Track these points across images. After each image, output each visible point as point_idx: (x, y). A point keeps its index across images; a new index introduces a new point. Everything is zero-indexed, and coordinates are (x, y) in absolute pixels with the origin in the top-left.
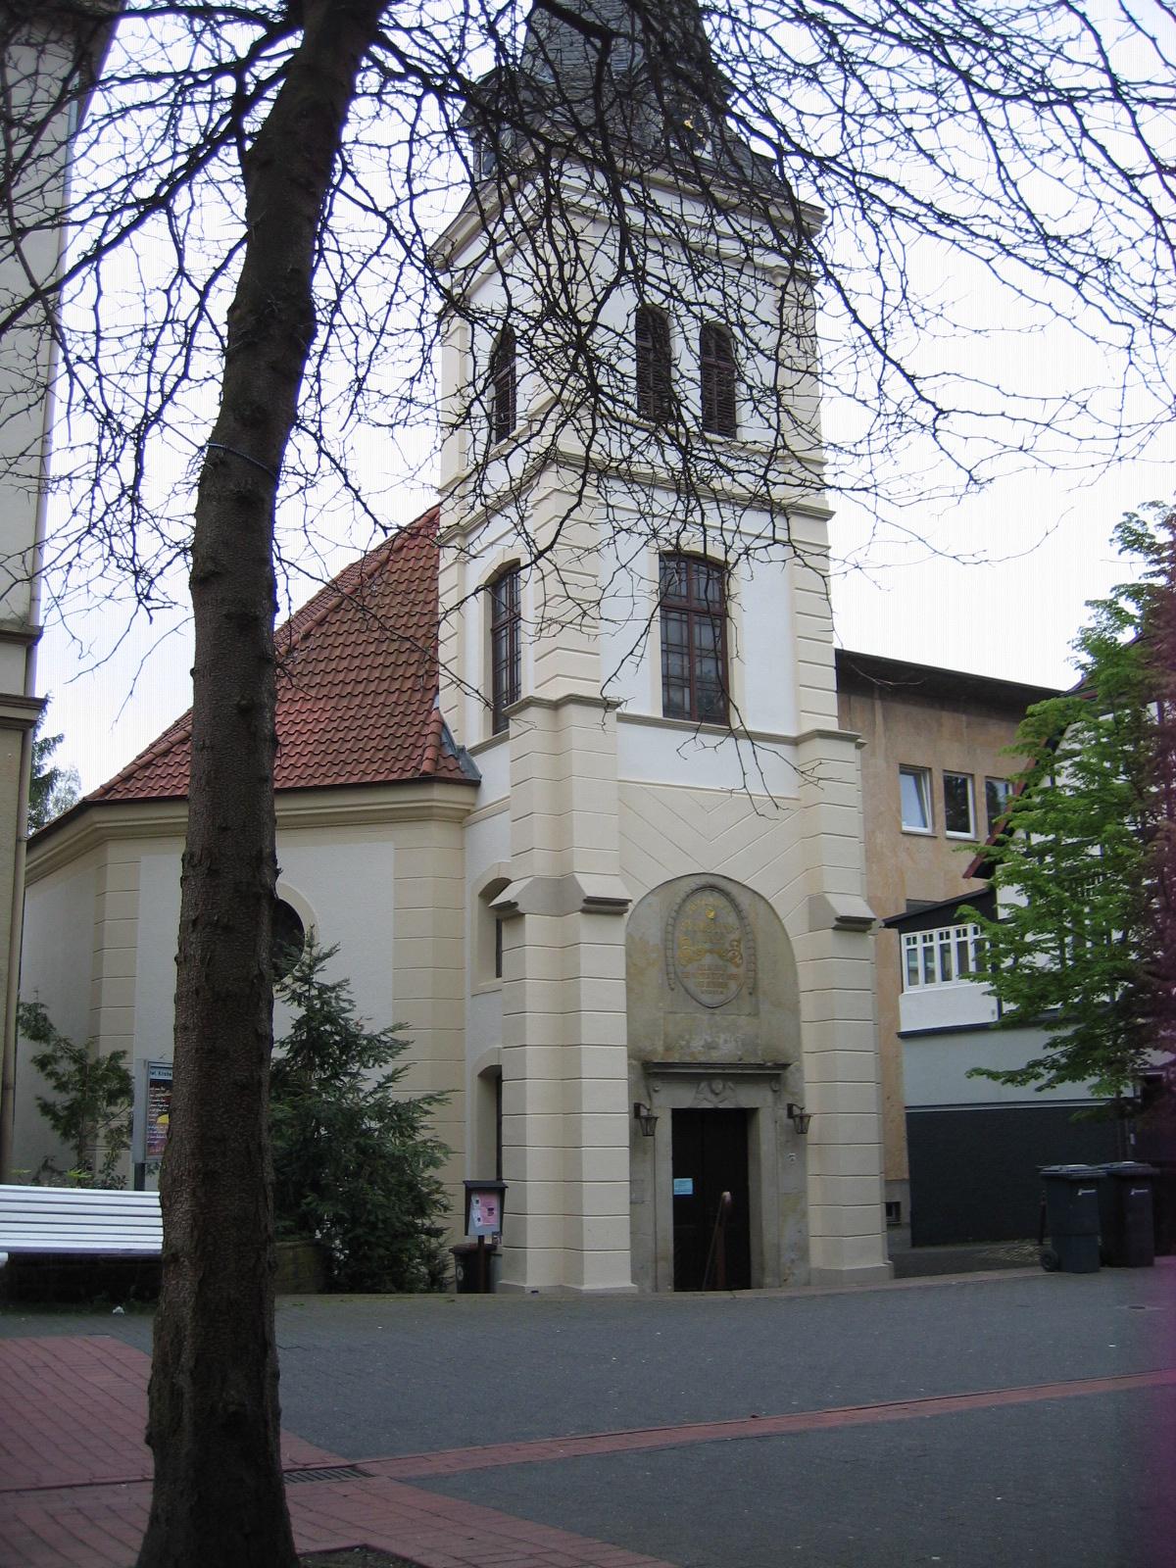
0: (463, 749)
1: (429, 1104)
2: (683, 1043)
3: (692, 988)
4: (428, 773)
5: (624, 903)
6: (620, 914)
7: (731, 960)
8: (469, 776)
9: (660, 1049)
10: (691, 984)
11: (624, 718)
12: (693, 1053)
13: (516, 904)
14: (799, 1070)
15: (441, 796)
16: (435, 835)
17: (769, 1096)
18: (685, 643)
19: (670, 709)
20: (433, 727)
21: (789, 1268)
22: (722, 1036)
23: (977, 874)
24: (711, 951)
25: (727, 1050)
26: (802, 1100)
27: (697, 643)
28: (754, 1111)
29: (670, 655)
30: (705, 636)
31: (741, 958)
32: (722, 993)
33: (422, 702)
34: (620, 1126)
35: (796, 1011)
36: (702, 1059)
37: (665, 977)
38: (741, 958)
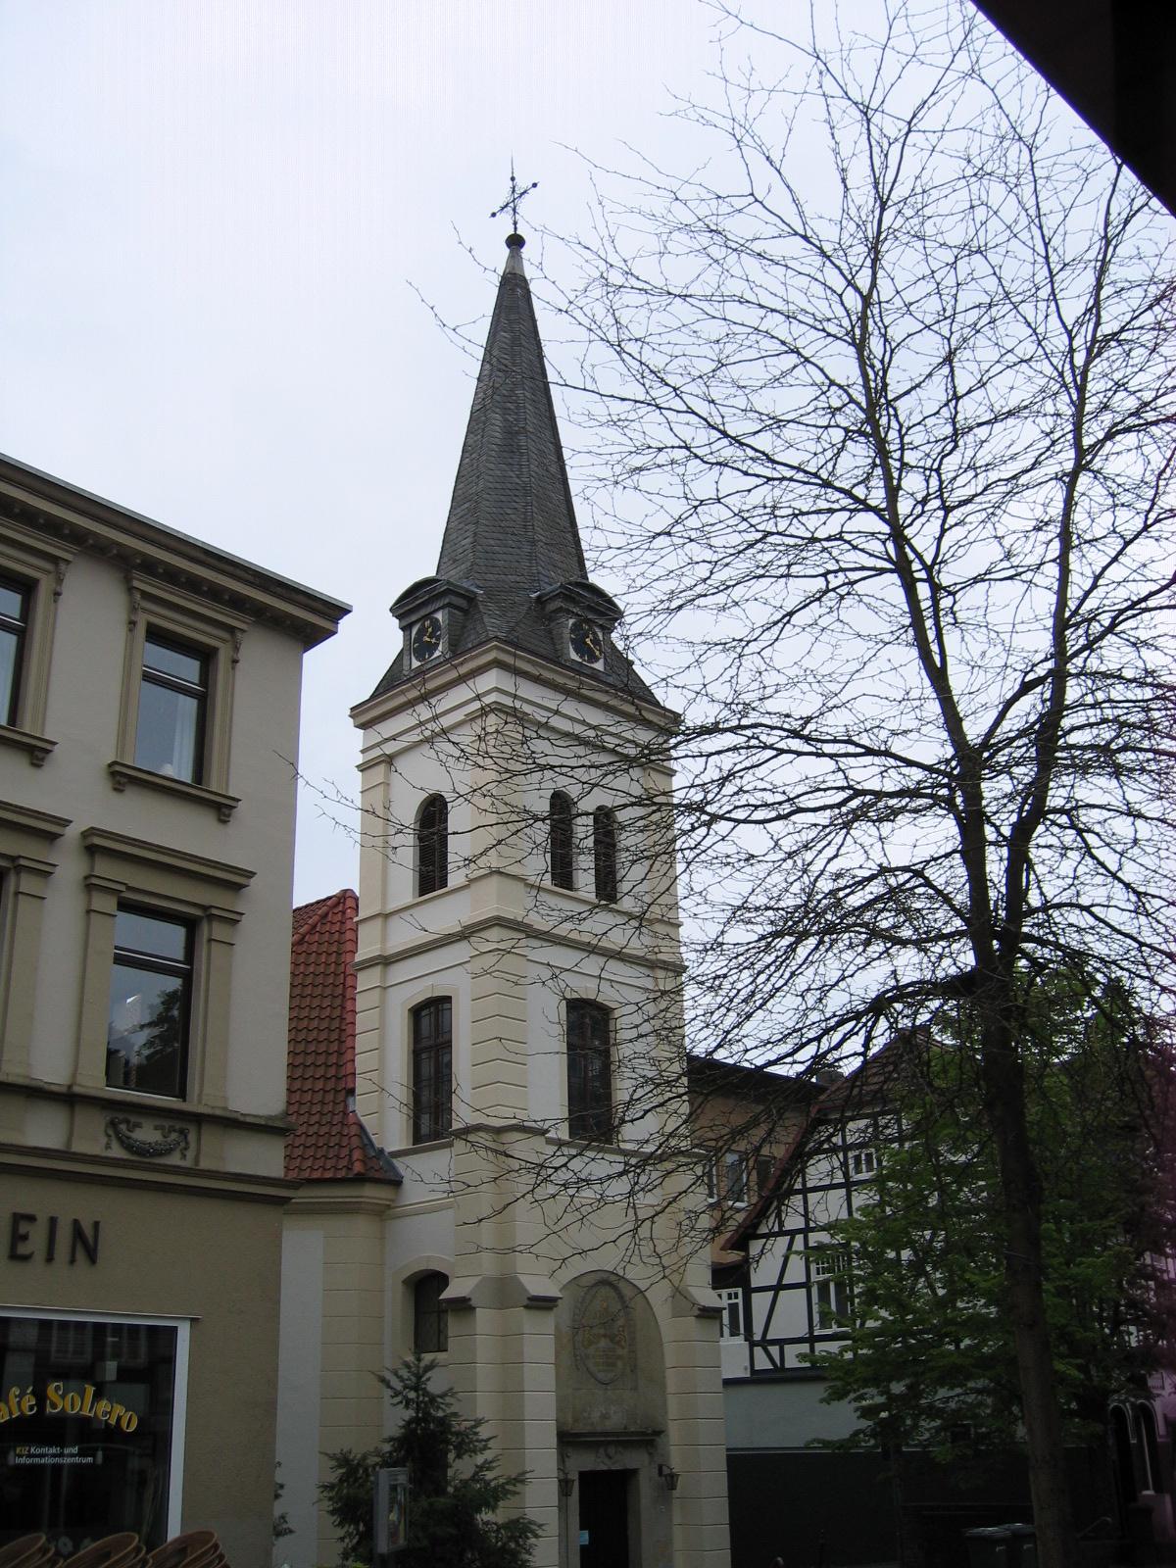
0: (382, 1151)
1: (515, 1485)
2: (585, 1415)
6: (550, 1309)
7: (618, 1343)
8: (391, 1176)
9: (570, 1420)
12: (592, 1424)
15: (371, 1193)
16: (360, 1227)
17: (645, 1457)
20: (354, 1130)
22: (613, 1408)
23: (733, 1248)
24: (605, 1336)
25: (616, 1421)
28: (634, 1472)
34: (553, 1487)
35: (663, 1386)
36: (599, 1429)
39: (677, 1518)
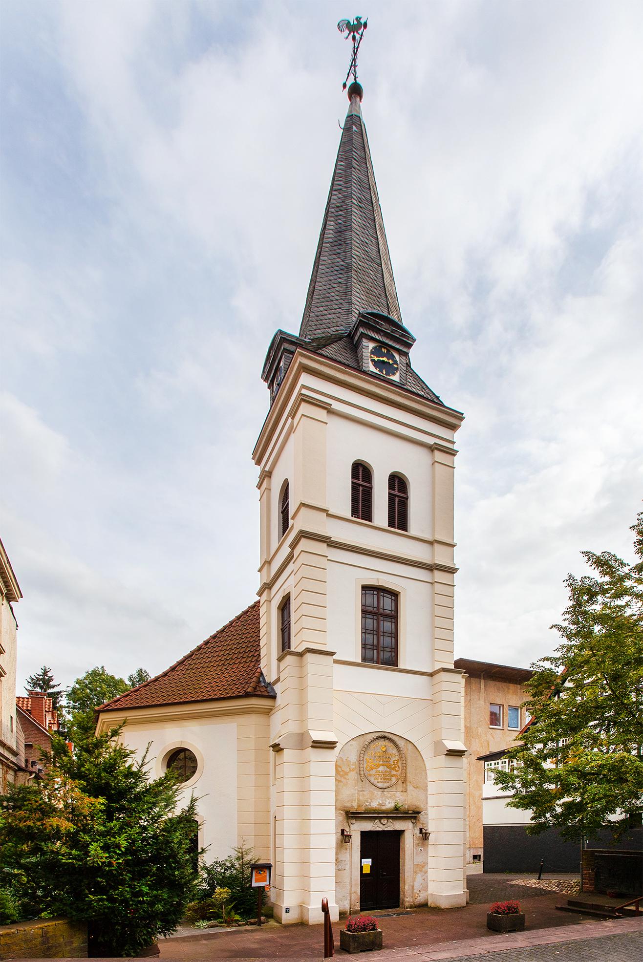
2: (367, 804)
3: (373, 780)
4: (249, 692)
5: (335, 743)
6: (333, 748)
7: (393, 769)
8: (272, 694)
9: (356, 807)
10: (372, 779)
11: (336, 662)
13: (279, 744)
14: (426, 814)
16: (252, 720)
18: (375, 629)
19: (364, 659)
21: (418, 894)
26: (427, 826)
27: (382, 630)
29: (366, 634)
30: (387, 626)
31: (399, 768)
32: (388, 782)
33: (254, 666)
34: (332, 840)
35: (425, 789)
37: (359, 776)
38: (399, 768)
39: (430, 854)
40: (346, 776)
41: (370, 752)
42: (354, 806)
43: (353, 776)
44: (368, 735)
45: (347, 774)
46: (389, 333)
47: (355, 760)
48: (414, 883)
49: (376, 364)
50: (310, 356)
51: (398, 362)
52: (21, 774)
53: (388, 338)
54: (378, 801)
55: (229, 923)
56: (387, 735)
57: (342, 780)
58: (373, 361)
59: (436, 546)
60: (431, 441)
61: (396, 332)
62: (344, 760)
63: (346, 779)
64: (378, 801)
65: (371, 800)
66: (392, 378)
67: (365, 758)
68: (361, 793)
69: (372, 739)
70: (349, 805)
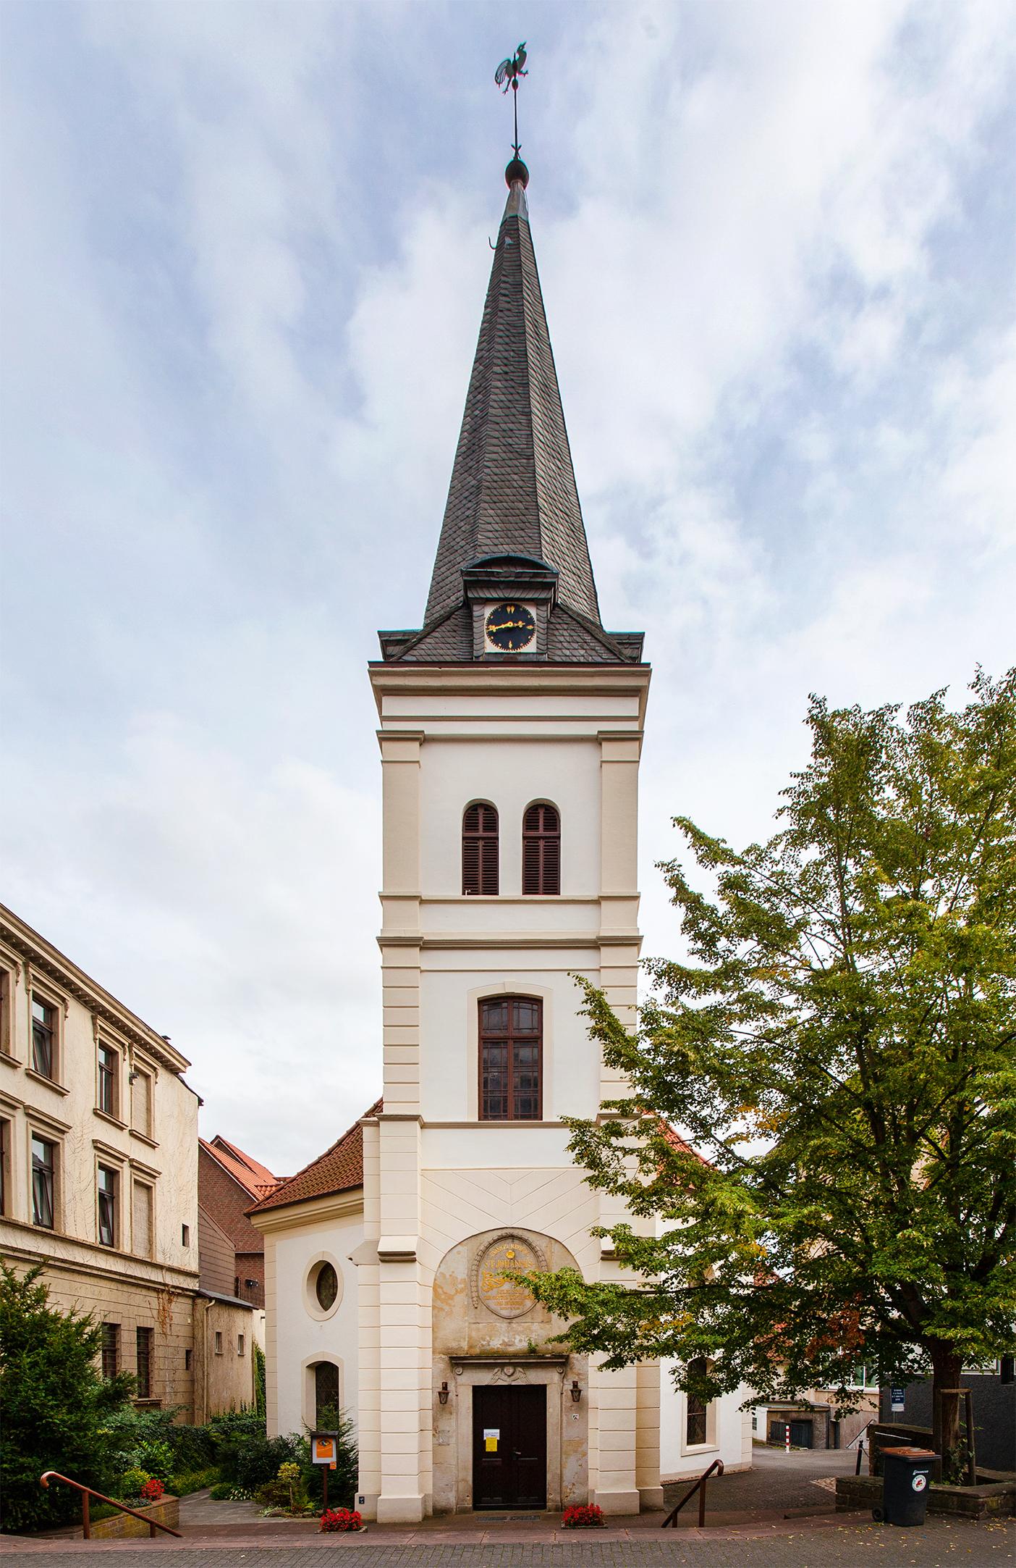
2: (484, 1343)
9: (466, 1348)
10: (492, 1304)
21: (571, 1489)
40: (450, 1302)
41: (489, 1262)
42: (463, 1347)
43: (461, 1300)
44: (486, 1235)
45: (451, 1297)
46: (513, 581)
47: (465, 1276)
48: (564, 1470)
49: (497, 638)
50: (388, 671)
51: (535, 619)
52: (199, 1301)
53: (512, 588)
54: (502, 1337)
55: (298, 1510)
56: (515, 1232)
57: (444, 1307)
58: (490, 634)
59: (603, 903)
60: (592, 729)
61: (531, 575)
62: (448, 1276)
63: (450, 1305)
64: (502, 1337)
65: (490, 1337)
66: (525, 649)
67: (480, 1272)
68: (474, 1326)
69: (486, 1244)
70: (454, 1345)
